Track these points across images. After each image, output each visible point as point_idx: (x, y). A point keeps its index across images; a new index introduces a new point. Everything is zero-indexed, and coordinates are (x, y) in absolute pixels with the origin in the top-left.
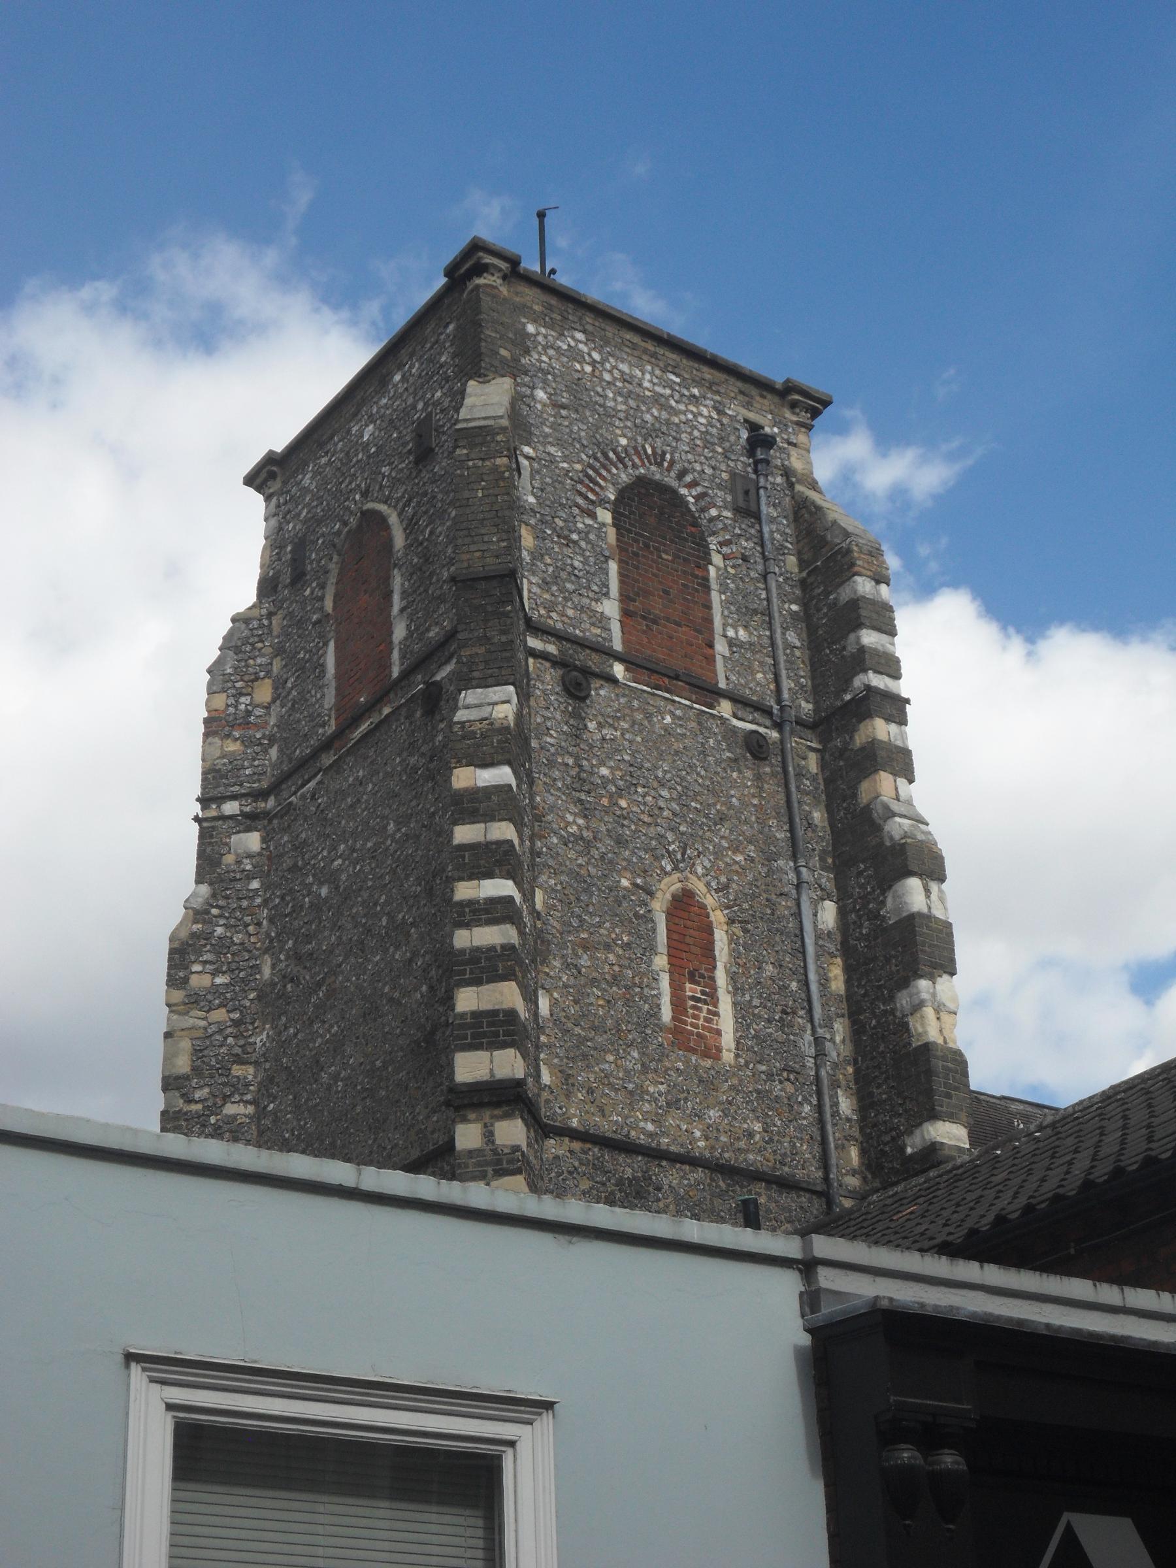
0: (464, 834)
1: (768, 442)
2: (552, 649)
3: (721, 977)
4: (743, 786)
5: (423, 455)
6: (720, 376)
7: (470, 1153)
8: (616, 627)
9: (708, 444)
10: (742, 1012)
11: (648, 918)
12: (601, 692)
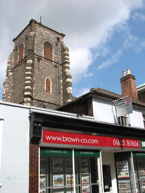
0: (27, 73)
1: (59, 39)
2: (37, 57)
3: (51, 87)
4: (54, 69)
5: (27, 39)
6: (55, 33)
7: (25, 101)
8: (43, 55)
9: (53, 39)
10: (53, 90)
11: (44, 81)
12: (41, 61)
